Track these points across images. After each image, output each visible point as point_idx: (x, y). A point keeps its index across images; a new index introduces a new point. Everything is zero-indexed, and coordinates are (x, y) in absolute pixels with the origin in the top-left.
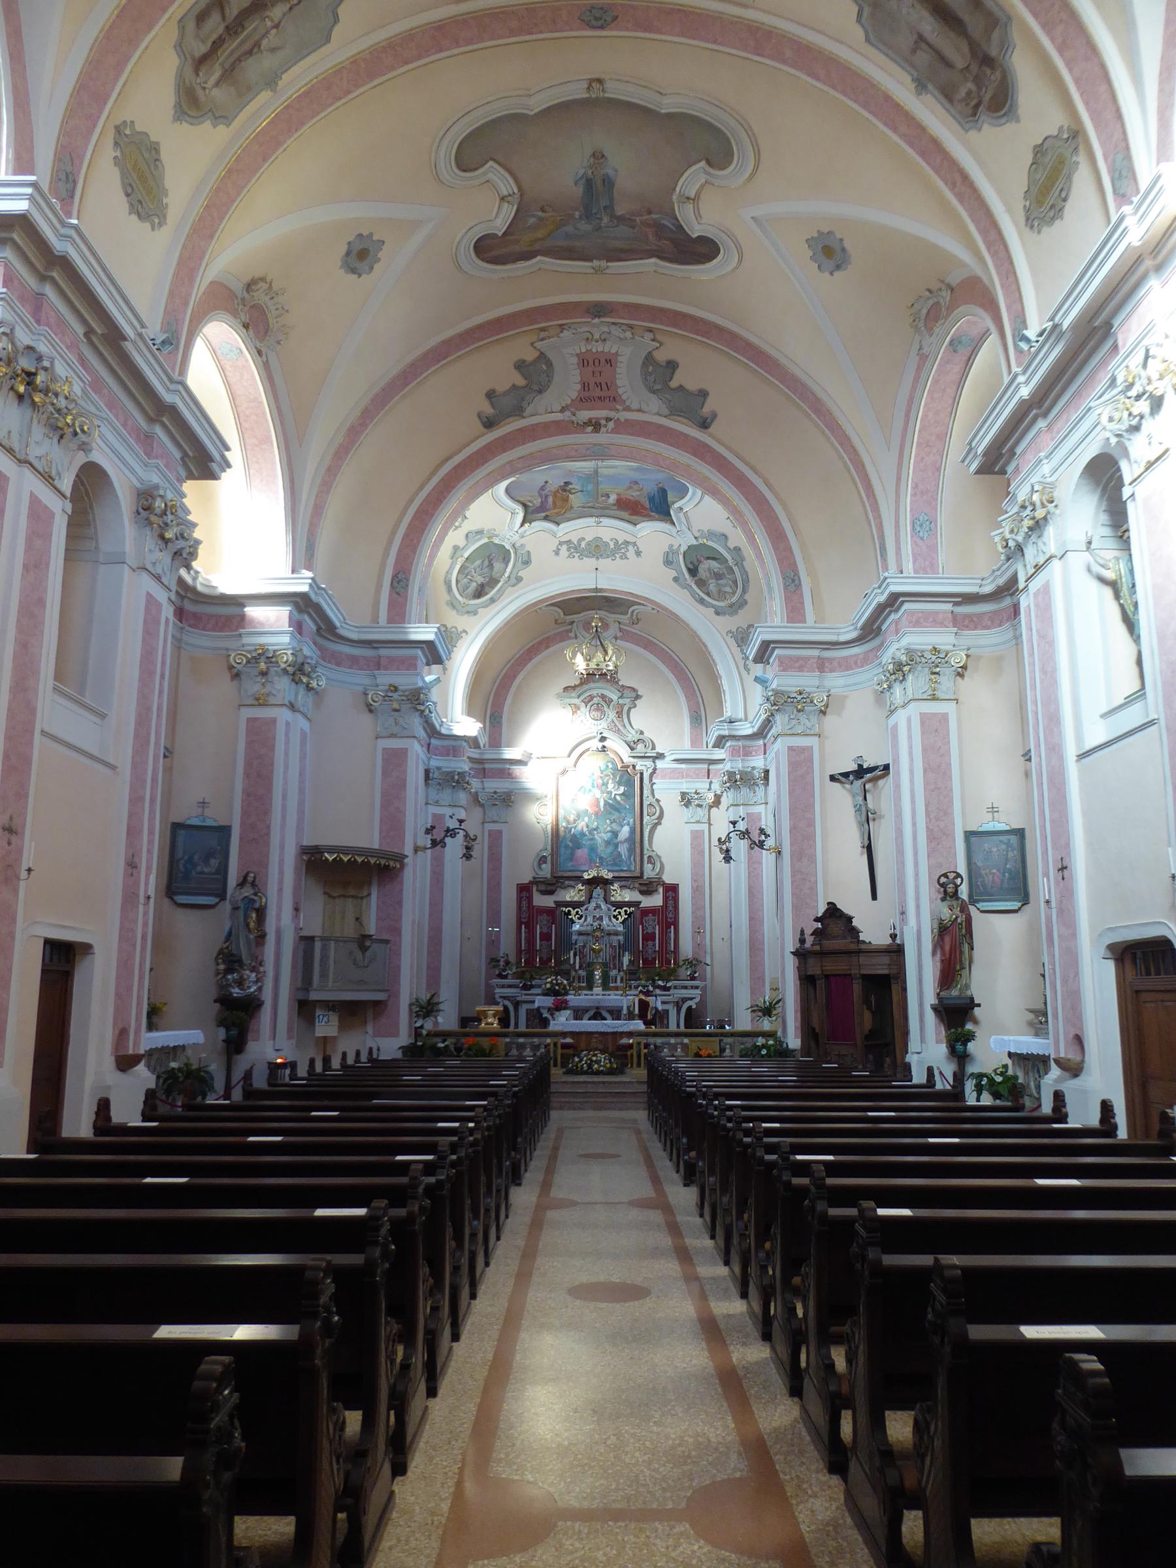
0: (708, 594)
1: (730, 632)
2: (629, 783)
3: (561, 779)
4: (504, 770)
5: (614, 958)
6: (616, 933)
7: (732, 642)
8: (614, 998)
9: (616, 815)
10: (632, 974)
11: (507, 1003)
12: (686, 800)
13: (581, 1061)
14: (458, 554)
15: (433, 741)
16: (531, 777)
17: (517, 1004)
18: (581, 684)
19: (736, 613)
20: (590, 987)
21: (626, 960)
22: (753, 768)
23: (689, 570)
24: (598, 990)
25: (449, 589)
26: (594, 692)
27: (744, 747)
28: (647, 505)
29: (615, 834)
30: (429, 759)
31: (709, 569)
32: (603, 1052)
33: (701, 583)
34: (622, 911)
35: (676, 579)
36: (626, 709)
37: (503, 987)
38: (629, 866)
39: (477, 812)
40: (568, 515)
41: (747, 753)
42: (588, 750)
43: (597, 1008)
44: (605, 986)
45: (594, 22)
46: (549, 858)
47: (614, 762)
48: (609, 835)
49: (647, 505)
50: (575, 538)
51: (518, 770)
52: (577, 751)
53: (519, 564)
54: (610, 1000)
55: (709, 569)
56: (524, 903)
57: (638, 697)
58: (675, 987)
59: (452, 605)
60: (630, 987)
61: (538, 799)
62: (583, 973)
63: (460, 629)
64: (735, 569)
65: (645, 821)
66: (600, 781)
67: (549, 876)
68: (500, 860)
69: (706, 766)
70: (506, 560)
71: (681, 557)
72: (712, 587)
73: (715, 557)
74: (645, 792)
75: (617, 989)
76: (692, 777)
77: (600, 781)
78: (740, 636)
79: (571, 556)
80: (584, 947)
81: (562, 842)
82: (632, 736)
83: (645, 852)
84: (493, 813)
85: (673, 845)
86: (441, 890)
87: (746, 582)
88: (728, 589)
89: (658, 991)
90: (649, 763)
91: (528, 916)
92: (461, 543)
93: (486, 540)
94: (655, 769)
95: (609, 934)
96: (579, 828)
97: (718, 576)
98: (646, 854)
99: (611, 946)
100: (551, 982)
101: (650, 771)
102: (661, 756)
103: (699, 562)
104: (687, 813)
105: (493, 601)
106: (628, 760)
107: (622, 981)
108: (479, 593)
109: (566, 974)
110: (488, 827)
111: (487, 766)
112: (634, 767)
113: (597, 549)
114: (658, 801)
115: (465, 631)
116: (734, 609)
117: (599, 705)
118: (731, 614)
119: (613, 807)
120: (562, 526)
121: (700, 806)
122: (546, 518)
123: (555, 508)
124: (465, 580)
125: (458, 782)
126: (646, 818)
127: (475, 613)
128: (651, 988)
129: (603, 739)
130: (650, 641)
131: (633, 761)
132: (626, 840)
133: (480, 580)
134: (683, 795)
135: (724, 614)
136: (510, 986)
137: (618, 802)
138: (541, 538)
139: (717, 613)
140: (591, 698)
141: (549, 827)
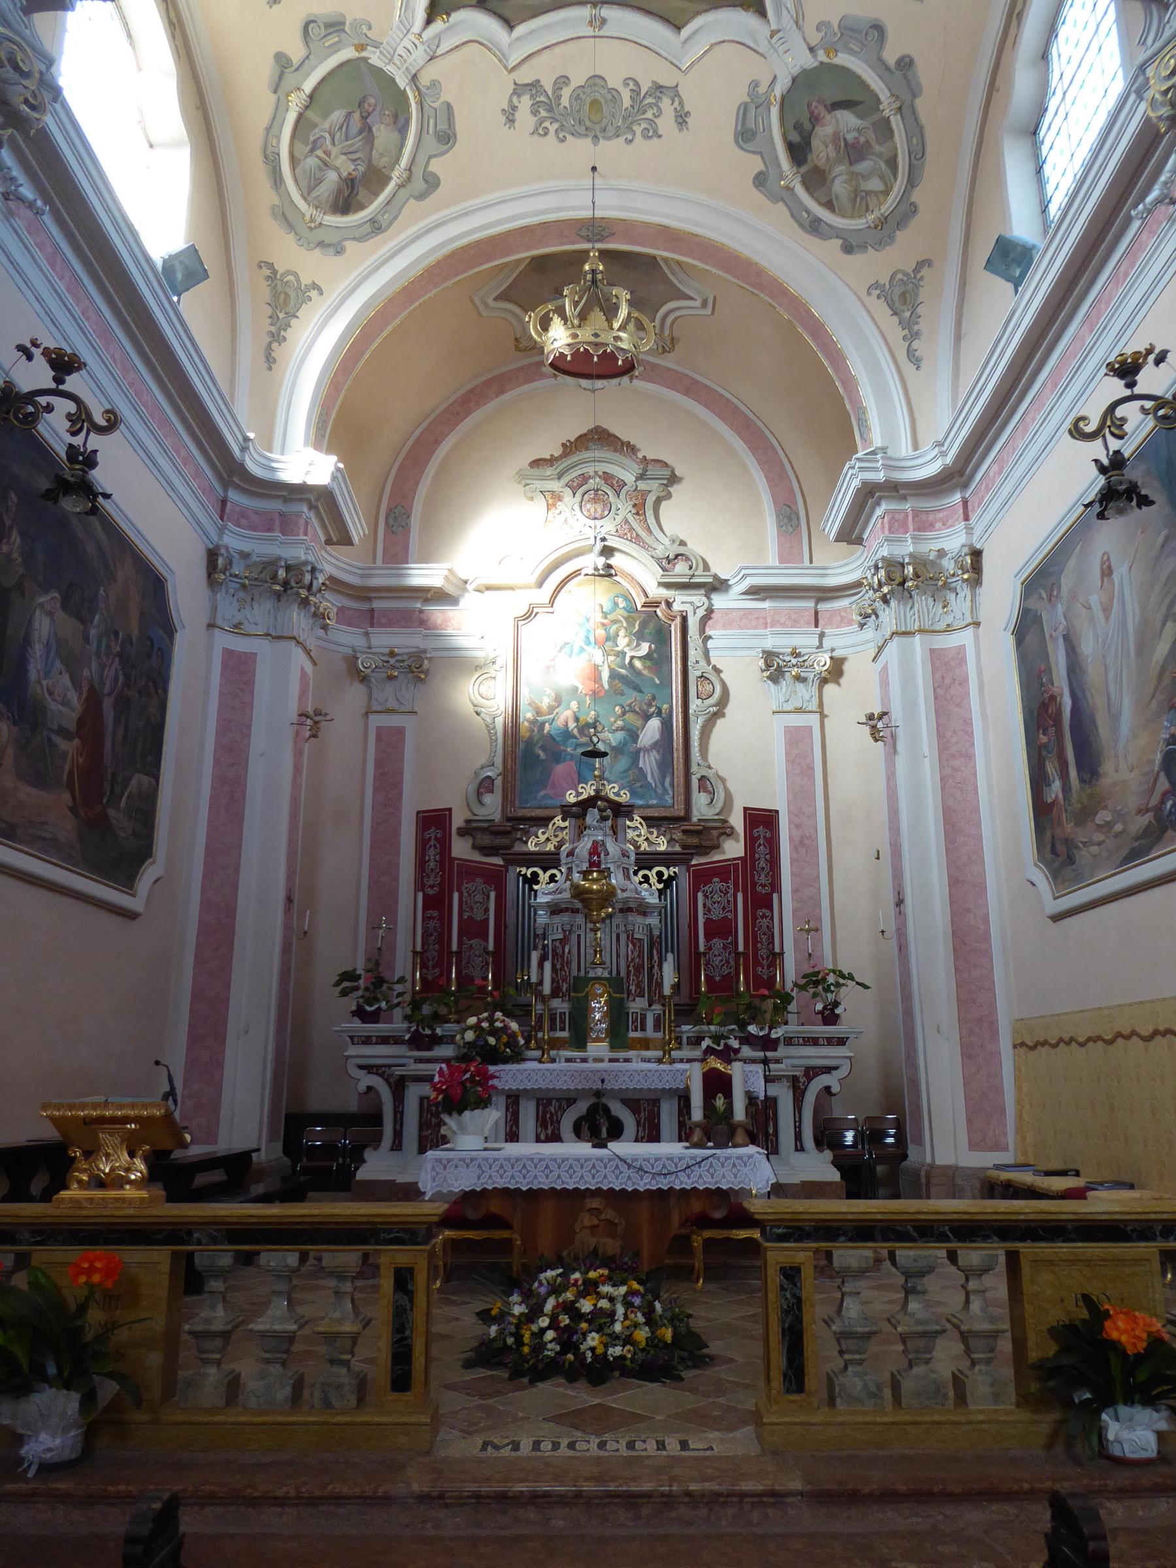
0: (829, 205)
2: (661, 637)
3: (526, 629)
4: (415, 607)
5: (639, 968)
6: (643, 909)
7: (881, 309)
8: (640, 1070)
9: (631, 697)
10: (686, 1009)
11: (376, 1081)
12: (775, 668)
13: (535, 1312)
14: (290, 80)
15: (233, 495)
16: (470, 626)
17: (399, 1086)
18: (565, 455)
19: (891, 238)
20: (580, 1040)
21: (669, 975)
22: (941, 553)
24: (598, 1048)
25: (277, 180)
26: (589, 470)
27: (917, 513)
29: (634, 735)
30: (221, 531)
32: (618, 1271)
33: (816, 180)
34: (652, 875)
35: (760, 180)
36: (651, 499)
37: (367, 1041)
38: (660, 798)
39: (355, 695)
41: (923, 524)
42: (576, 573)
43: (598, 1094)
44: (618, 1037)
46: (498, 782)
47: (628, 598)
48: (620, 735)
50: (543, 71)
51: (438, 613)
52: (556, 575)
54: (631, 1074)
55: (836, 136)
56: (432, 854)
57: (673, 479)
58: (789, 1041)
59: (286, 217)
60: (678, 1040)
61: (477, 667)
62: (561, 1005)
63: (305, 280)
64: (896, 122)
65: (692, 708)
66: (601, 632)
67: (497, 817)
68: (398, 785)
69: (810, 604)
70: (400, 123)
71: (775, 111)
72: (840, 188)
73: (854, 98)
74: (692, 653)
75: (645, 1044)
76: (783, 625)
77: (601, 632)
78: (897, 292)
79: (540, 131)
80: (564, 941)
81: (528, 754)
82: (665, 548)
83: (694, 768)
84: (386, 694)
85: (745, 757)
86: (238, 820)
87: (918, 155)
88: (875, 184)
89: (747, 1052)
90: (698, 598)
91: (440, 881)
93: (348, 53)
94: (710, 611)
95: (626, 910)
96: (560, 722)
97: (854, 152)
98: (696, 772)
99: (631, 938)
100: (477, 1027)
101: (701, 612)
102: (718, 586)
103: (815, 120)
104: (776, 694)
105: (376, 227)
106: (656, 592)
107: (657, 1027)
108: (345, 202)
109: (522, 1012)
110: (376, 721)
111: (376, 604)
112: (669, 605)
113: (592, 113)
114: (717, 671)
115: (315, 286)
116: (886, 230)
117: (598, 493)
118: (879, 245)
119: (625, 680)
120: (520, 30)
121: (799, 679)
124: (312, 162)
125: (286, 584)
126: (695, 704)
127: (340, 251)
128: (735, 1044)
129: (607, 551)
130: (695, 382)
131: (664, 593)
132: (655, 746)
133: (346, 166)
134: (769, 656)
135: (863, 247)
136: (384, 1040)
137: (638, 673)
139: (848, 249)
140: (584, 479)
141: (499, 722)
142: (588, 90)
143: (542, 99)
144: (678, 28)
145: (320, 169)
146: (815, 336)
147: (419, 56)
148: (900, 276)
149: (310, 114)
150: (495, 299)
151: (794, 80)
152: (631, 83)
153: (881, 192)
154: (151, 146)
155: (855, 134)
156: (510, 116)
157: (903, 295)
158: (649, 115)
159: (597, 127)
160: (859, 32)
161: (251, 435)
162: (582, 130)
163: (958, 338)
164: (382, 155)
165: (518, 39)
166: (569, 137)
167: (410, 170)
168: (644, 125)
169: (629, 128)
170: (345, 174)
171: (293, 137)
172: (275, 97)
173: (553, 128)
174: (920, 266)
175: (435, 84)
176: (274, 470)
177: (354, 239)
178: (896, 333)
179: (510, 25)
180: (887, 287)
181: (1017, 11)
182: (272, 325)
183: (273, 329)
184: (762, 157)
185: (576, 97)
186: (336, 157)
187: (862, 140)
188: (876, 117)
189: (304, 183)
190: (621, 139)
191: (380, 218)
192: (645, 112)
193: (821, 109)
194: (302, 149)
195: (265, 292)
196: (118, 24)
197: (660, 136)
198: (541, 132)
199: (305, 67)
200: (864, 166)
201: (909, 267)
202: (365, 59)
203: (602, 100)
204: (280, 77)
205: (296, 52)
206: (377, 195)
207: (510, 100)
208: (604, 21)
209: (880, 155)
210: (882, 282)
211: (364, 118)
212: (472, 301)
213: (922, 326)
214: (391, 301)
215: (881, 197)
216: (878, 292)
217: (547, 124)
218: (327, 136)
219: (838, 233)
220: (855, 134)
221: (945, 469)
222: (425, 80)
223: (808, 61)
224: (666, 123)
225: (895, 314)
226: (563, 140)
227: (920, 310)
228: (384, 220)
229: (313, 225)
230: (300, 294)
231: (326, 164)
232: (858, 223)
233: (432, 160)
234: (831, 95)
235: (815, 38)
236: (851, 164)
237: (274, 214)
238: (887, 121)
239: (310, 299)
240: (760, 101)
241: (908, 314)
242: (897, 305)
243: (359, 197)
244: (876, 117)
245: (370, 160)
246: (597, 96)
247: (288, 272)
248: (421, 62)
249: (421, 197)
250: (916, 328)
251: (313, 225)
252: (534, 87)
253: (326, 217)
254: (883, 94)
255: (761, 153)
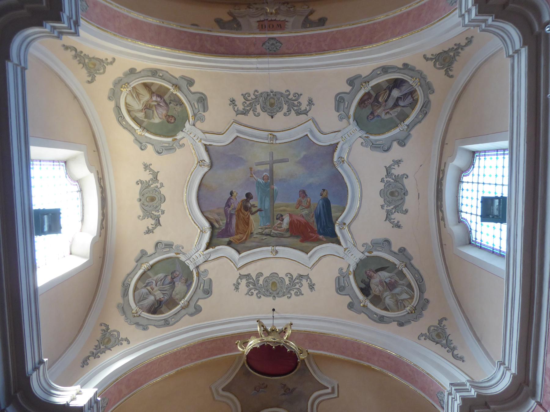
0: (386, 309)
1: (422, 335)
14: (144, 259)
23: (362, 290)
25: (125, 294)
28: (315, 226)
31: (381, 282)
33: (377, 300)
35: (351, 306)
40: (248, 244)
45: (274, 42)
49: (315, 226)
50: (252, 270)
53: (200, 292)
55: (381, 282)
59: (123, 309)
64: (405, 271)
70: (188, 282)
71: (351, 277)
72: (388, 300)
73: (384, 266)
78: (434, 335)
87: (420, 281)
88: (405, 296)
92: (150, 250)
97: (391, 286)
103: (370, 277)
105: (167, 323)
108: (155, 309)
113: (273, 287)
118: (416, 319)
122: (229, 244)
123: (237, 234)
124: (144, 291)
127: (145, 328)
133: (159, 295)
135: (409, 322)
138: (225, 265)
139: (401, 324)
142: (271, 278)
143: (251, 281)
144: (307, 254)
145: (147, 294)
146: (396, 372)
147: (201, 260)
148: (432, 328)
149: (149, 272)
150: (223, 390)
151: (357, 265)
152: (289, 275)
153: (409, 298)
154: (71, 254)
155: (389, 279)
156: (237, 287)
157: (438, 335)
158: (297, 286)
159: (275, 293)
160: (380, 244)
161: (45, 360)
162: (268, 294)
163: (479, 340)
164: (177, 294)
165: (242, 257)
166: (262, 296)
167: (189, 302)
168: (295, 291)
169: (289, 292)
170: (158, 298)
171: (139, 279)
172: (136, 264)
173: (255, 292)
174: (440, 321)
175: (206, 271)
176: (52, 395)
177: (155, 326)
178: (444, 351)
179: (239, 252)
180: (428, 334)
181: (440, 218)
182: (95, 349)
183: (94, 351)
184: (350, 297)
185: (266, 280)
186: (156, 291)
187: (393, 280)
188: (396, 271)
189: (137, 298)
190: (286, 297)
191: (170, 320)
192: (295, 285)
193: (372, 274)
194: (141, 285)
195: (99, 336)
196: (79, 203)
197: (303, 294)
198: (250, 293)
199: (153, 256)
200: (397, 290)
201: (436, 323)
202: (178, 258)
203: (277, 282)
204: (141, 258)
205: (150, 250)
206: (170, 310)
207: (237, 280)
208: (277, 252)
209: (403, 285)
210: (424, 333)
211: (172, 279)
212: (210, 388)
213: (455, 343)
214: (165, 358)
215: (409, 300)
216: (424, 337)
217: (253, 291)
218: (154, 282)
219: (393, 320)
220: (389, 279)
221: (514, 377)
222: (202, 269)
223: (361, 256)
224: (305, 288)
225: (437, 343)
226: (260, 297)
227: (450, 338)
228: (172, 321)
229: (136, 315)
230: (117, 341)
231: (150, 292)
232: (402, 313)
233: (200, 300)
234: (374, 267)
235: (363, 249)
236: (391, 290)
237: (118, 306)
238: (402, 271)
239: (122, 344)
240: (344, 275)
241: (445, 342)
242: (437, 339)
243: (162, 309)
244: (396, 271)
245: (171, 295)
246: (274, 280)
247: (114, 331)
248: (201, 262)
249: (192, 315)
250: (452, 346)
251: (136, 315)
252: (248, 276)
253: (143, 313)
254: (397, 262)
255: (348, 295)
